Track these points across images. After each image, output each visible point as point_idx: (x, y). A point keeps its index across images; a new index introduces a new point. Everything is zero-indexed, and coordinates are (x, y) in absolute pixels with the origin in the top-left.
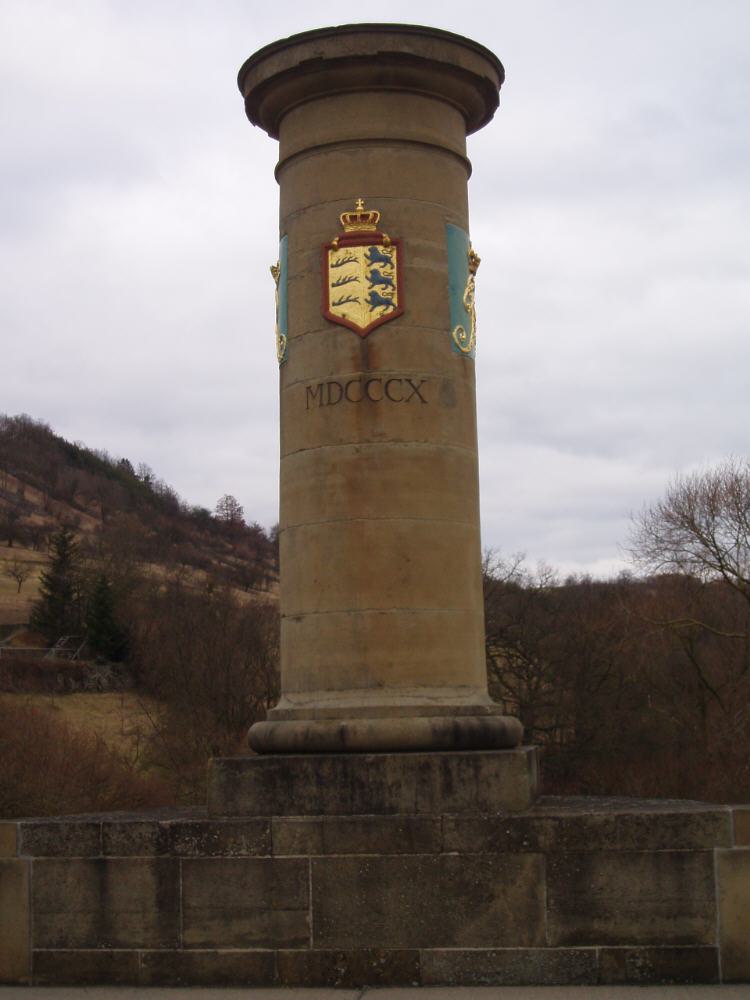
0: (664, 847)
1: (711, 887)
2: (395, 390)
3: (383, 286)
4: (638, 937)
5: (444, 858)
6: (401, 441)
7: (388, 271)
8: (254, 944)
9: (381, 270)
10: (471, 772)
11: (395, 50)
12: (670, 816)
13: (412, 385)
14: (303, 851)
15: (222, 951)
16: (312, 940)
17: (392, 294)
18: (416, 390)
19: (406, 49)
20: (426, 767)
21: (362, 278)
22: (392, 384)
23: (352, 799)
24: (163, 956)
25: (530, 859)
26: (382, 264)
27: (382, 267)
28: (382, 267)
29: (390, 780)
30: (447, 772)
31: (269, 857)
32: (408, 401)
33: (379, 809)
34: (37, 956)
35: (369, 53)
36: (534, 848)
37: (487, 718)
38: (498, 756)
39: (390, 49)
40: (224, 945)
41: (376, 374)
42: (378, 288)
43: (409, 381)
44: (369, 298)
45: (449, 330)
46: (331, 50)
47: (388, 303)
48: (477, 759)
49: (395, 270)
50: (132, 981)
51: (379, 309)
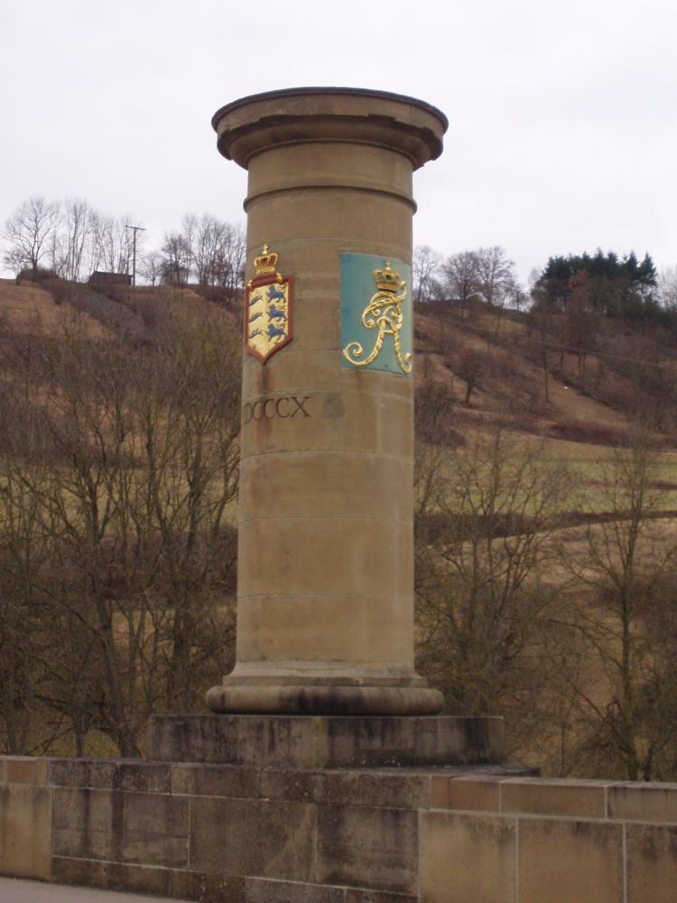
0: (388, 805)
1: (416, 844)
2: (284, 408)
3: (278, 318)
4: (370, 882)
5: (261, 802)
6: (286, 451)
7: (282, 305)
8: (159, 863)
9: (276, 305)
10: (285, 732)
11: (272, 114)
12: (393, 778)
13: (297, 402)
14: (186, 791)
15: (144, 866)
16: (189, 863)
17: (284, 325)
18: (300, 406)
19: (280, 112)
20: (260, 727)
21: (264, 314)
22: (281, 403)
23: (220, 751)
24: (114, 867)
25: (309, 808)
26: (277, 299)
27: (278, 302)
28: (278, 302)
29: (241, 736)
30: (272, 732)
31: (168, 794)
32: (292, 416)
33: (233, 760)
34: (55, 859)
35: (254, 121)
36: (311, 799)
37: (361, 688)
38: (302, 720)
39: (268, 114)
40: (145, 861)
41: (270, 395)
42: (274, 321)
43: (294, 398)
44: (268, 330)
45: (338, 349)
46: (339, 108)
47: (280, 332)
48: (289, 722)
49: (287, 304)
50: (97, 885)
51: (275, 339)
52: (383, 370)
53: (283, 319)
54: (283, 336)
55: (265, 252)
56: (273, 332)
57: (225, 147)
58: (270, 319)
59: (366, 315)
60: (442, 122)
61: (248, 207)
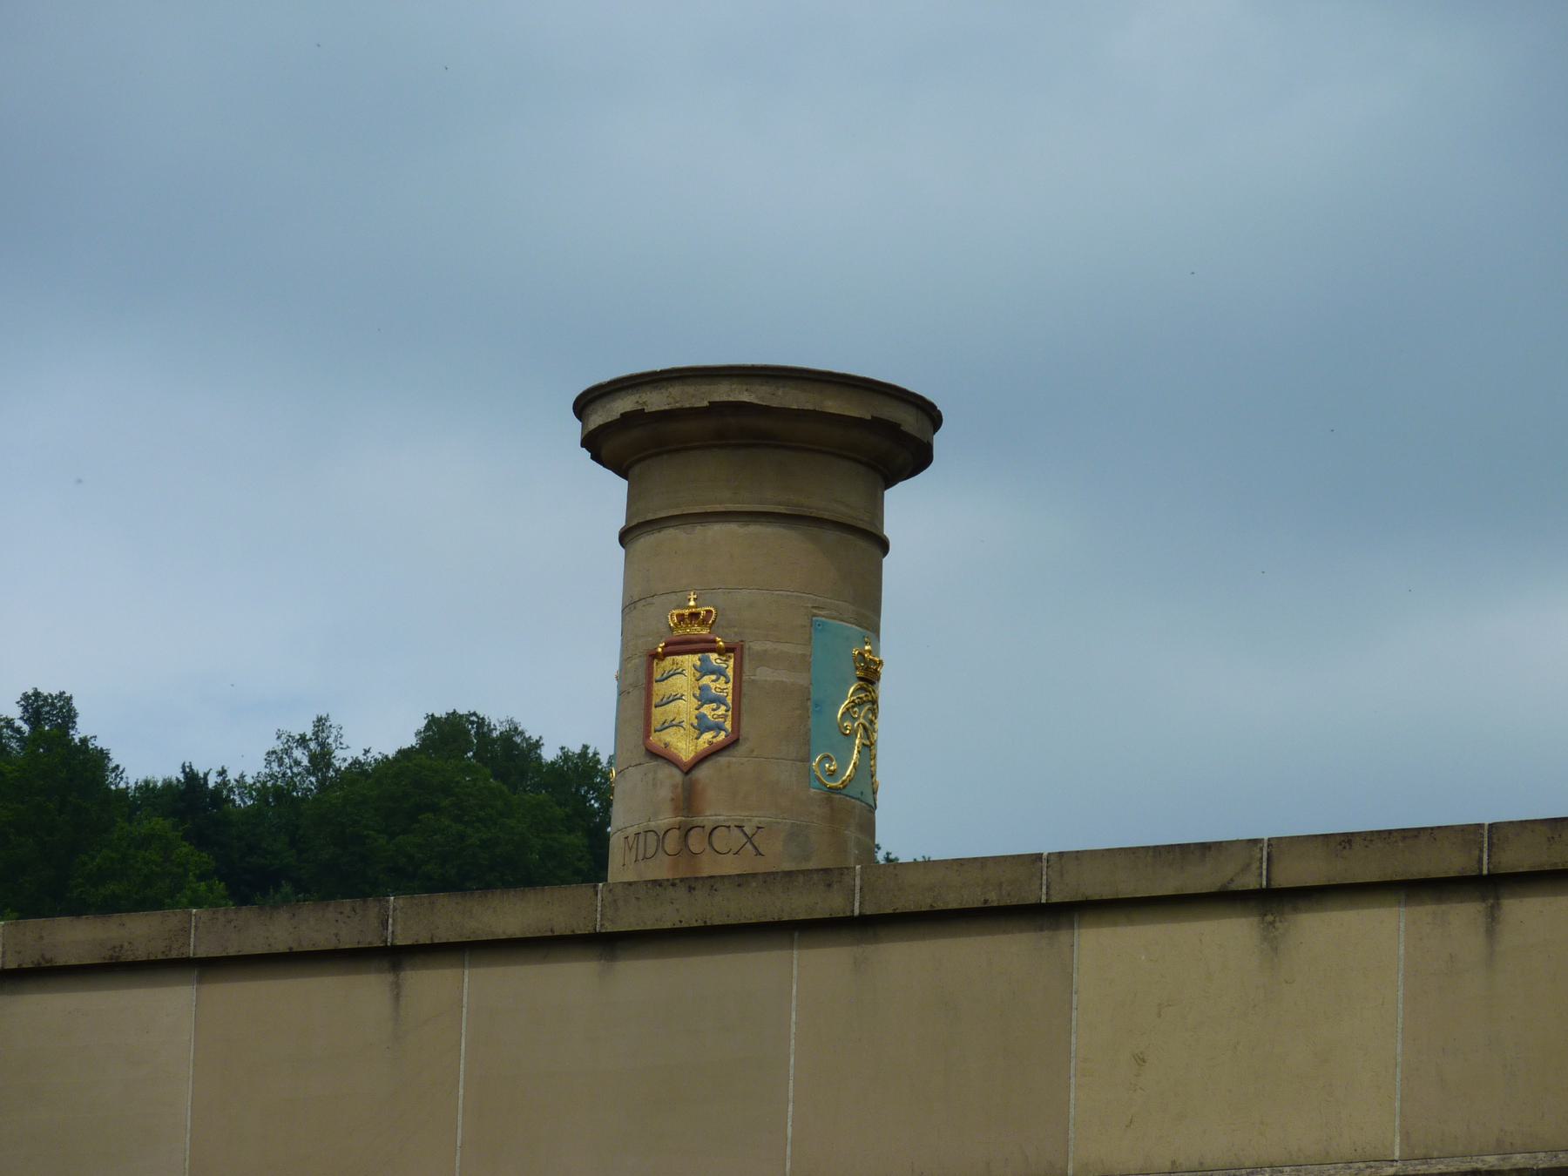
3: (714, 705)
7: (721, 687)
9: (713, 685)
17: (725, 716)
18: (750, 839)
21: (688, 696)
22: (716, 832)
26: (714, 677)
41: (698, 820)
43: (740, 827)
47: (718, 728)
49: (730, 685)
51: (708, 736)
52: (858, 799)
53: (723, 708)
54: (723, 734)
55: (692, 603)
56: (703, 726)
57: (594, 443)
58: (701, 706)
59: (843, 714)
60: (933, 417)
61: (627, 540)
